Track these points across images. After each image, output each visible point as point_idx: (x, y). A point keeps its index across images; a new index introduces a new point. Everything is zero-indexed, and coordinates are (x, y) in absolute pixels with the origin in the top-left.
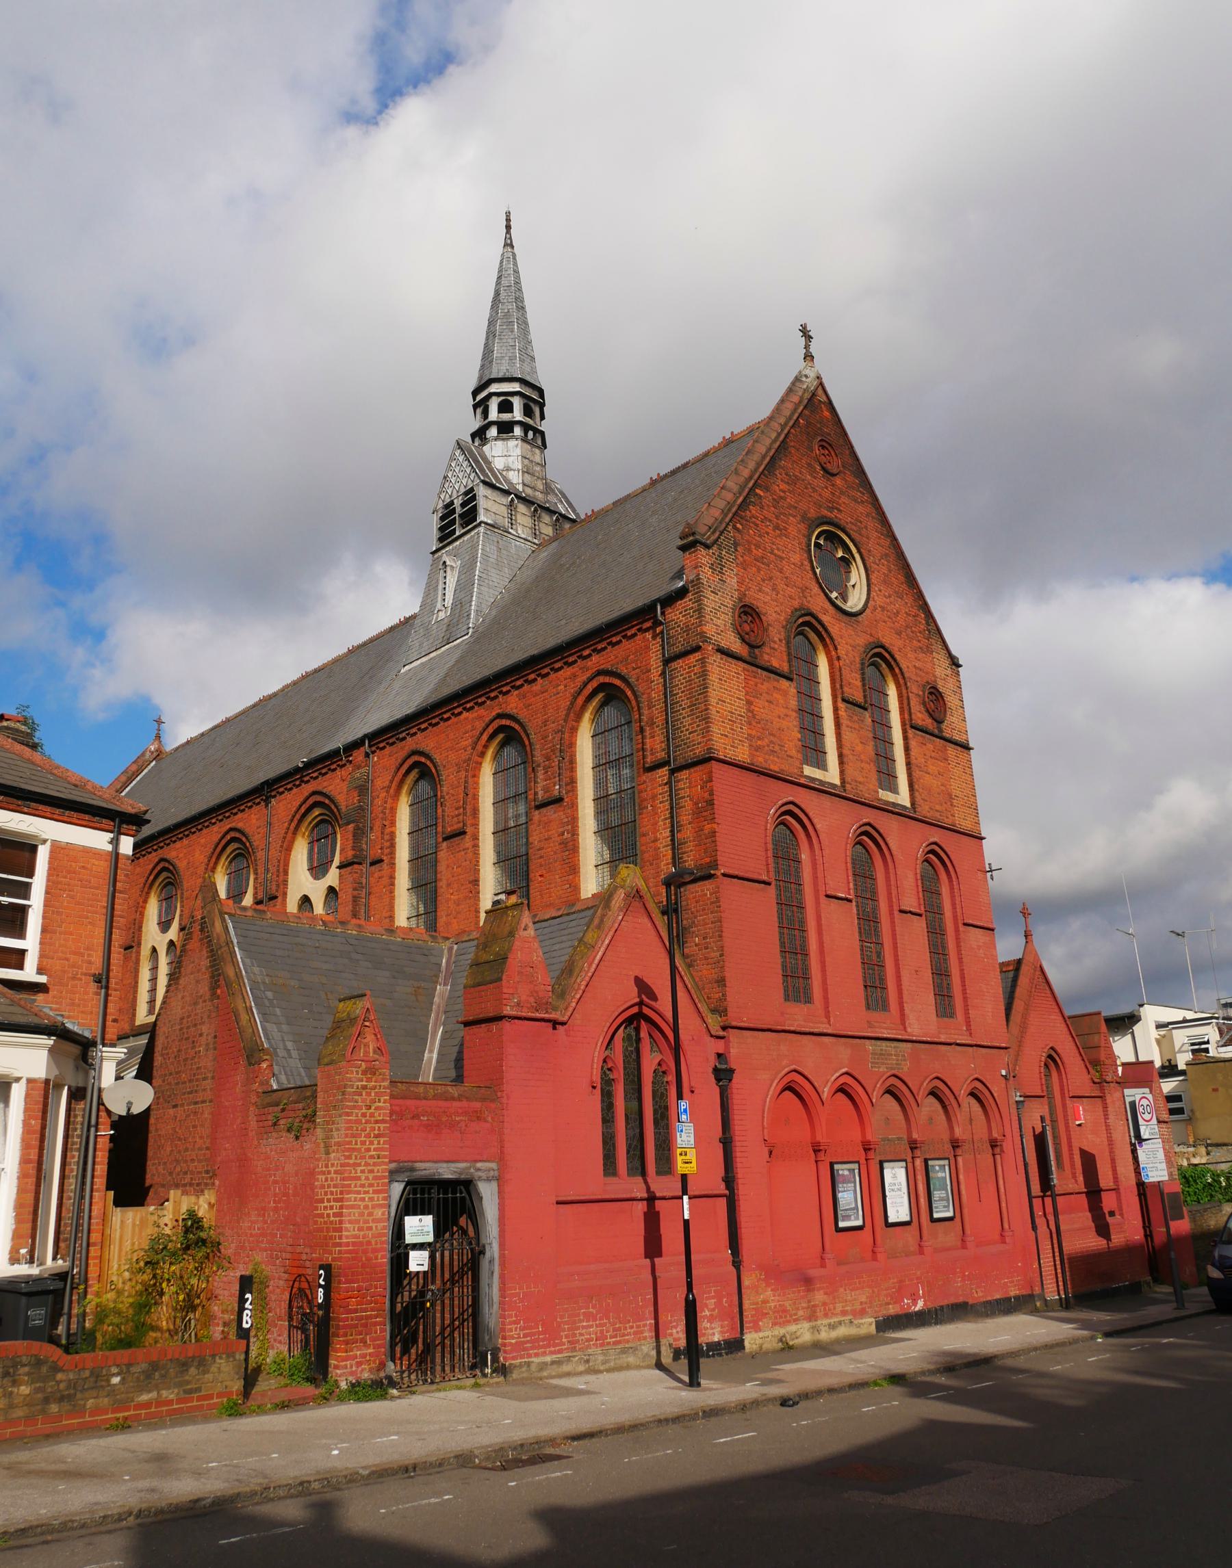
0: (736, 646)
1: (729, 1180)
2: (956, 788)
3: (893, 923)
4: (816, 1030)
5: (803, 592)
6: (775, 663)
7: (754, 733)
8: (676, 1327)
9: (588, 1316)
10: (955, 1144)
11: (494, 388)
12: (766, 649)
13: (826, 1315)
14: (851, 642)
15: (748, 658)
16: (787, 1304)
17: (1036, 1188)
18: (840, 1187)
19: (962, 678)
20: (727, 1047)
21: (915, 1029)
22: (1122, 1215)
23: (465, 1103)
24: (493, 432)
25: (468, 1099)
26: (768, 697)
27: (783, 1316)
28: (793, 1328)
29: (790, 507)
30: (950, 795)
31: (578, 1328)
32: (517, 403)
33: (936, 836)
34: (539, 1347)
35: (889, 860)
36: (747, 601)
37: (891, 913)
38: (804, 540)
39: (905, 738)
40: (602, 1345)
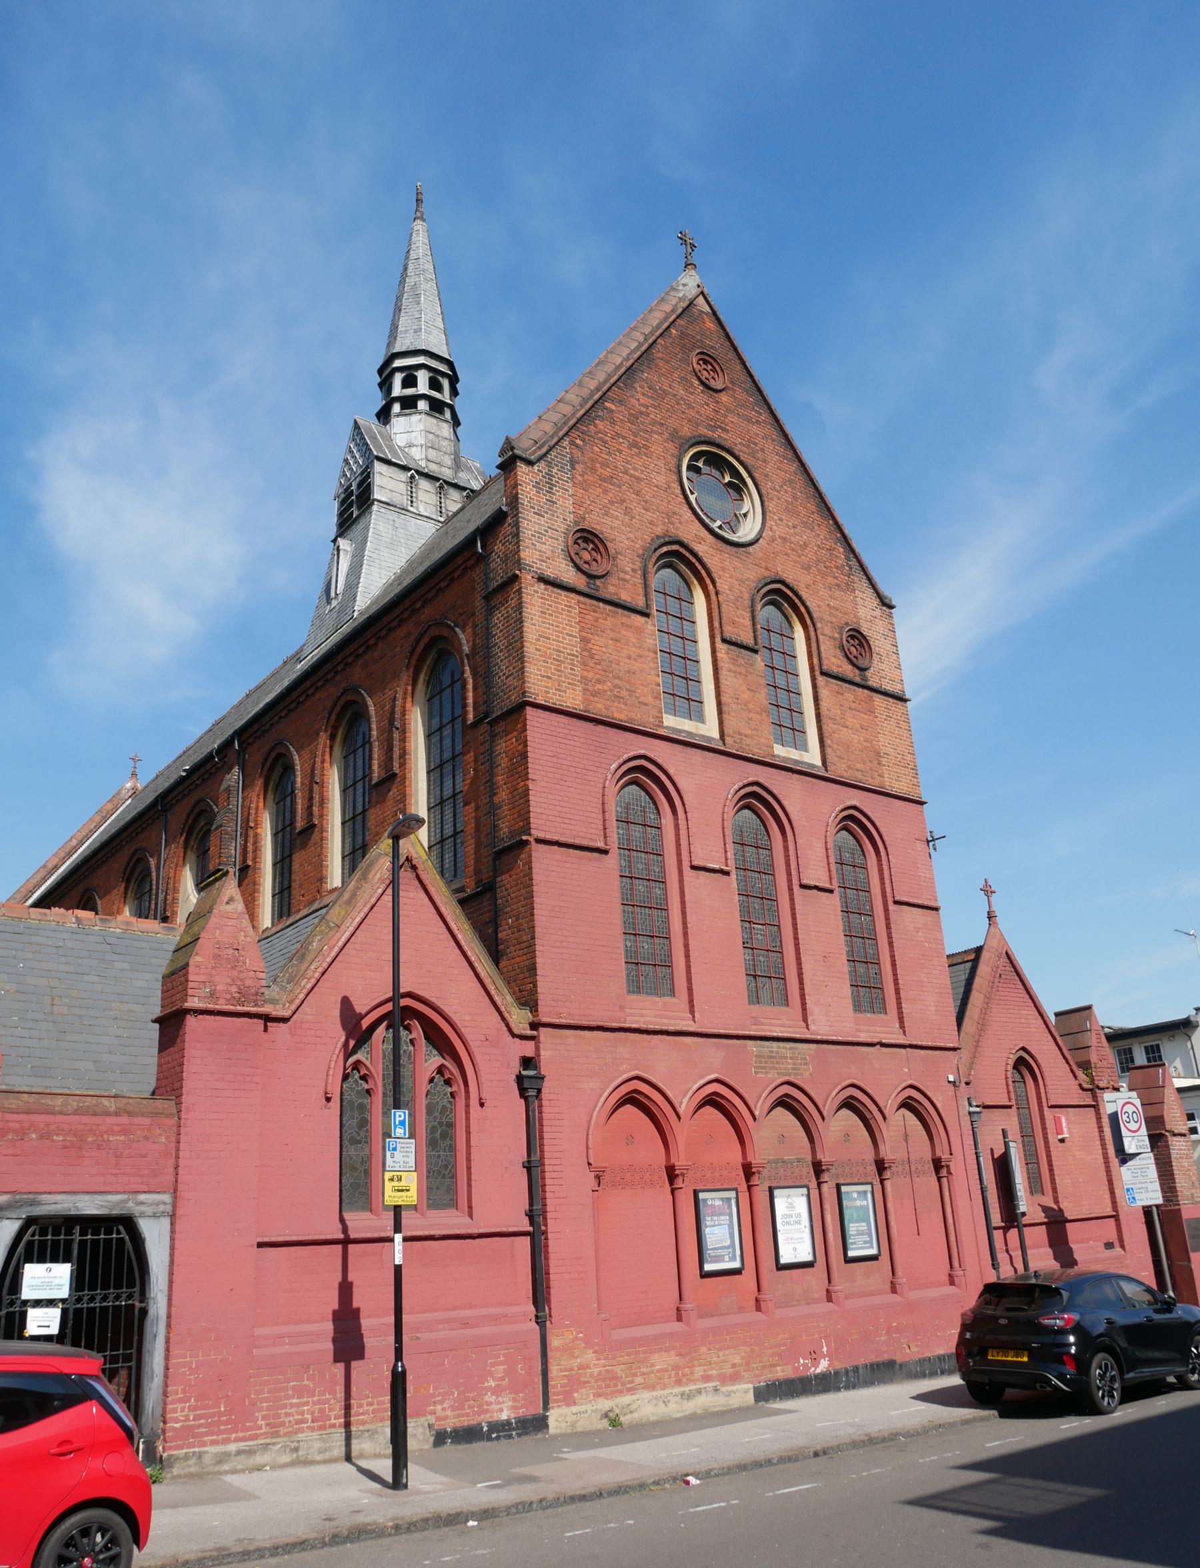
0: (569, 575)
1: (536, 1214)
2: (884, 742)
3: (792, 899)
4: (671, 1028)
5: (669, 517)
6: (625, 597)
7: (590, 675)
8: (441, 1402)
9: (300, 1392)
10: (881, 1166)
11: (398, 363)
12: (613, 580)
13: (678, 1382)
14: (735, 577)
15: (587, 590)
16: (619, 1370)
17: (996, 1220)
18: (707, 1221)
19: (895, 620)
20: (537, 1048)
21: (821, 1027)
22: (1123, 1247)
23: (124, 1120)
24: (396, 408)
25: (130, 1114)
26: (612, 635)
27: (610, 1384)
28: (626, 1399)
29: (654, 423)
30: (878, 754)
31: (284, 1407)
32: (423, 377)
33: (855, 798)
34: (219, 1433)
35: (883, 853)
36: (585, 525)
37: (790, 889)
38: (673, 461)
39: (814, 686)
40: (322, 1428)
